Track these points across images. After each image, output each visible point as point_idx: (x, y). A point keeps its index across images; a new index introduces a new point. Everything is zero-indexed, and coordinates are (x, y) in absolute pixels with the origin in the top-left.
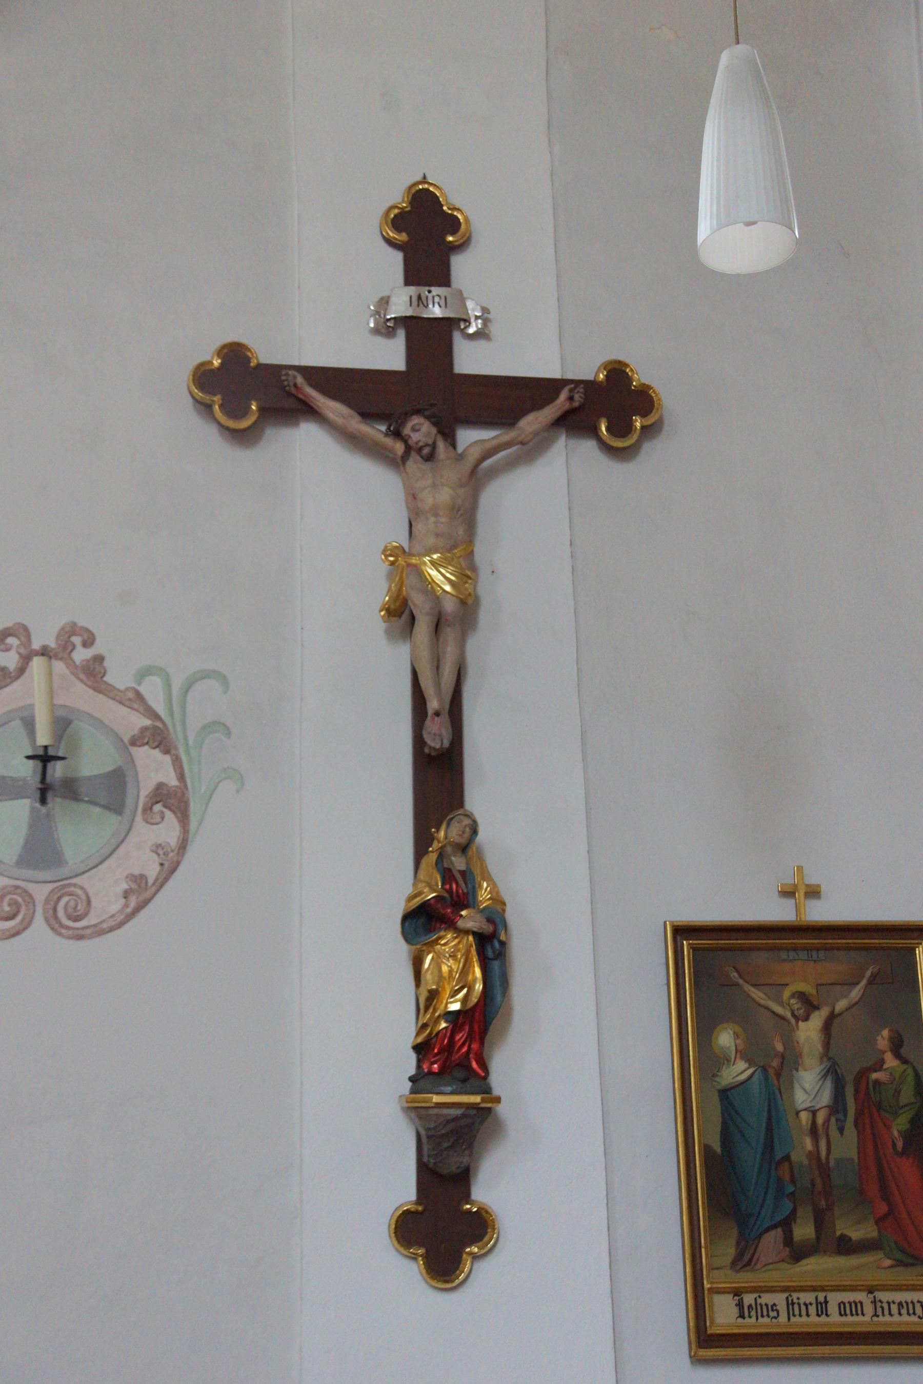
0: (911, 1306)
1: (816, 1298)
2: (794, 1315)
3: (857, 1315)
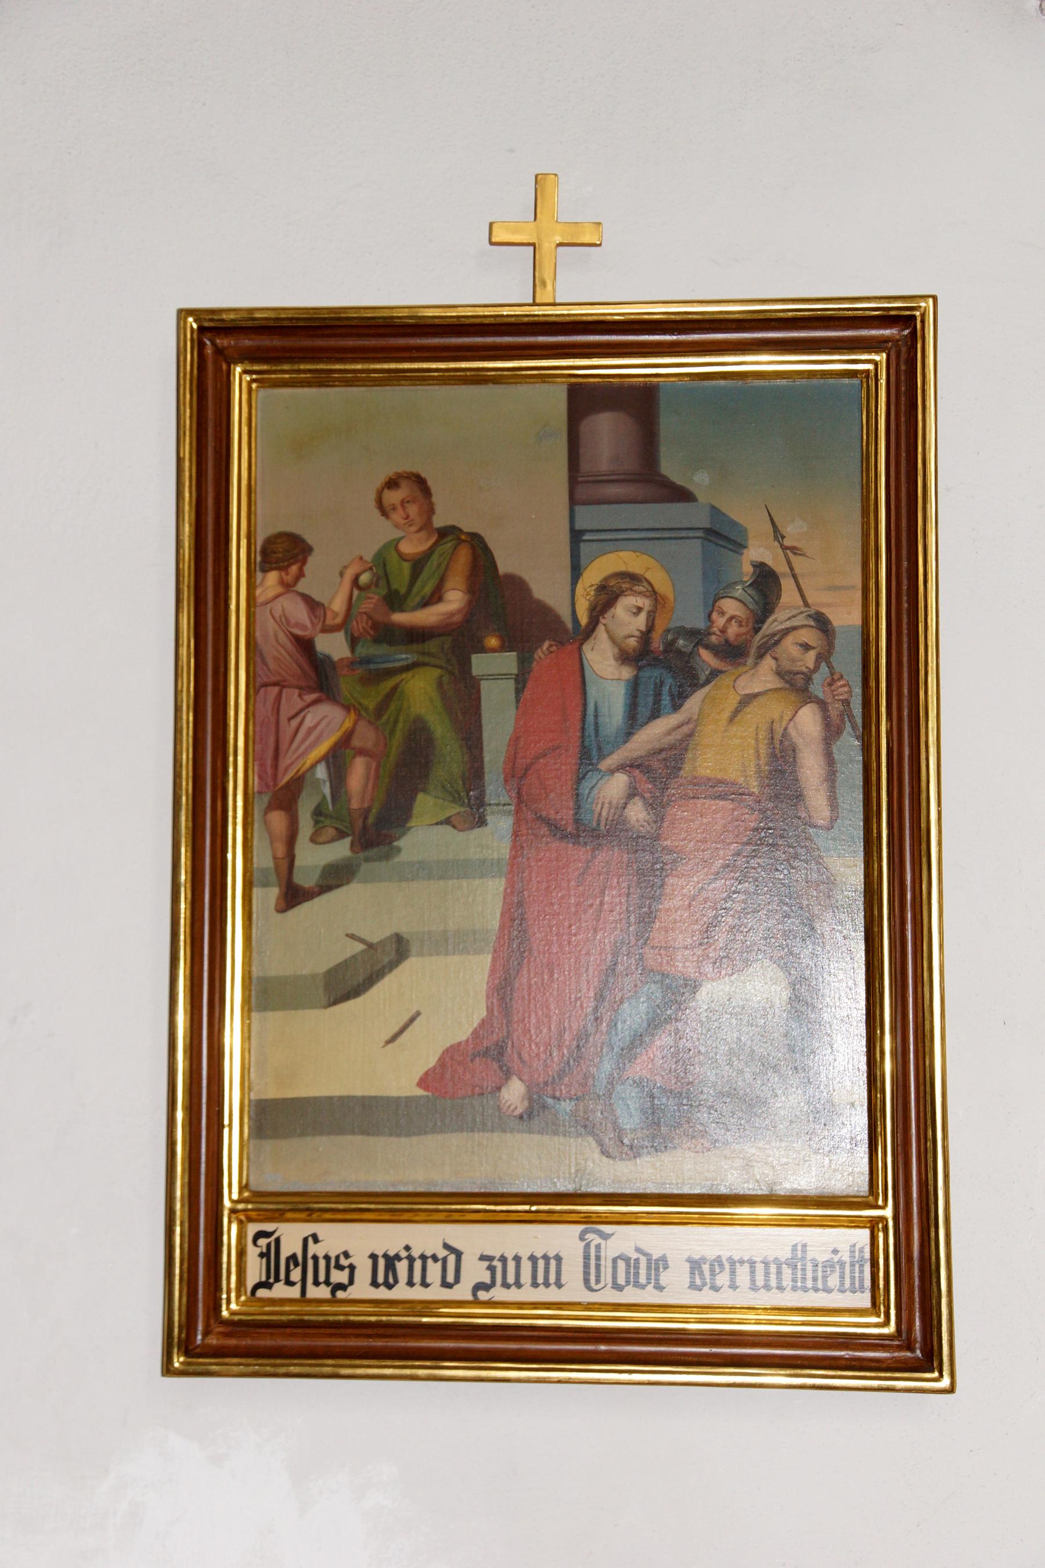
3: (547, 1284)
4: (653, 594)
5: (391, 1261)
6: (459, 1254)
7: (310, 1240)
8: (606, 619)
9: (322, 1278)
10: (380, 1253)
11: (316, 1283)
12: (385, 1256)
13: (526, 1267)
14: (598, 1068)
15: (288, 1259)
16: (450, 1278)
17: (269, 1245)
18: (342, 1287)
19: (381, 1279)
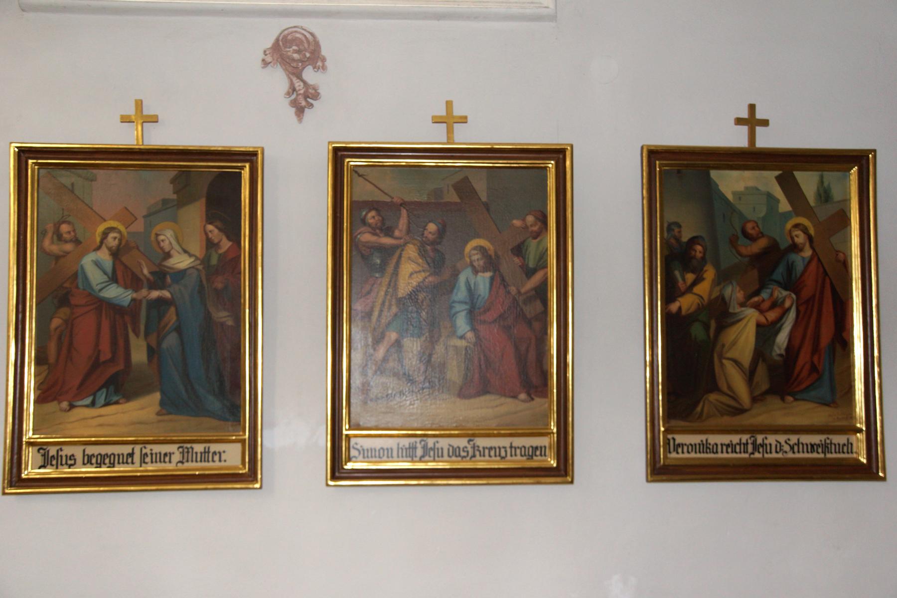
0: (498, 450)
1: (84, 451)
4: (120, 232)
5: (812, 446)
8: (105, 241)
9: (64, 462)
11: (119, 463)
13: (719, 447)
14: (107, 404)
18: (465, 457)
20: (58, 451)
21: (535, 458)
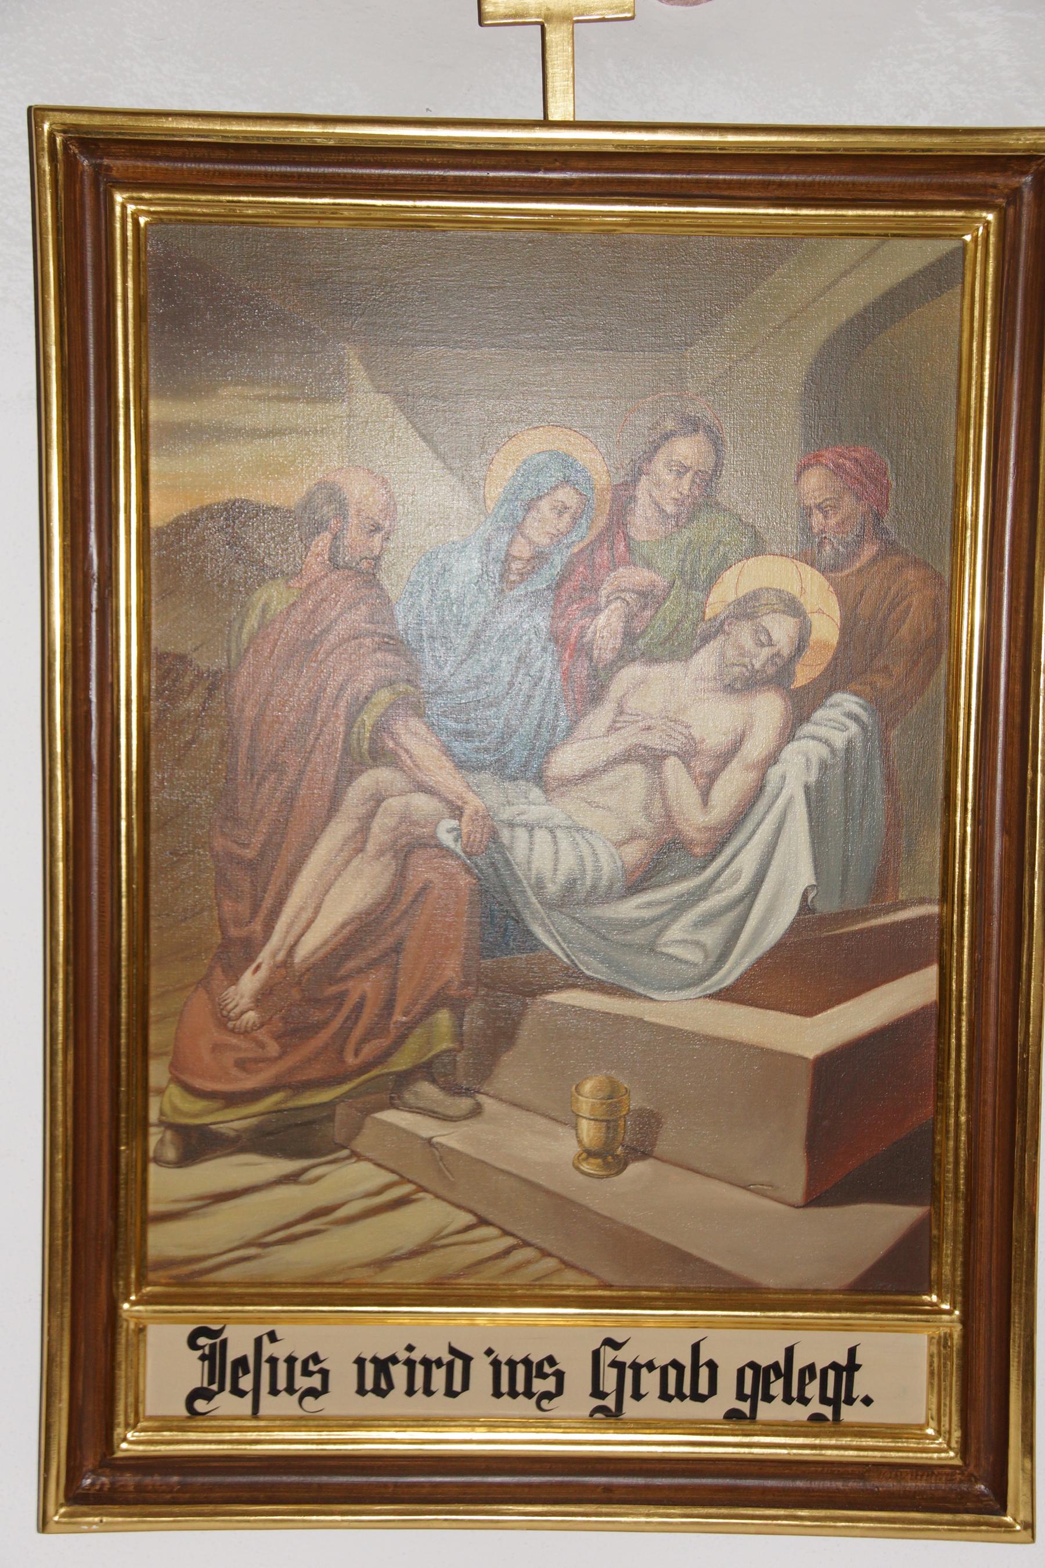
1: (696, 1348)
2: (637, 1395)
5: (383, 1366)
6: (467, 1360)
7: (265, 1339)
10: (368, 1356)
11: (274, 1391)
12: (375, 1360)
15: (802, 1372)
16: (457, 1386)
17: (213, 1347)
19: (369, 1384)
20: (258, 1342)
21: (765, 1412)
